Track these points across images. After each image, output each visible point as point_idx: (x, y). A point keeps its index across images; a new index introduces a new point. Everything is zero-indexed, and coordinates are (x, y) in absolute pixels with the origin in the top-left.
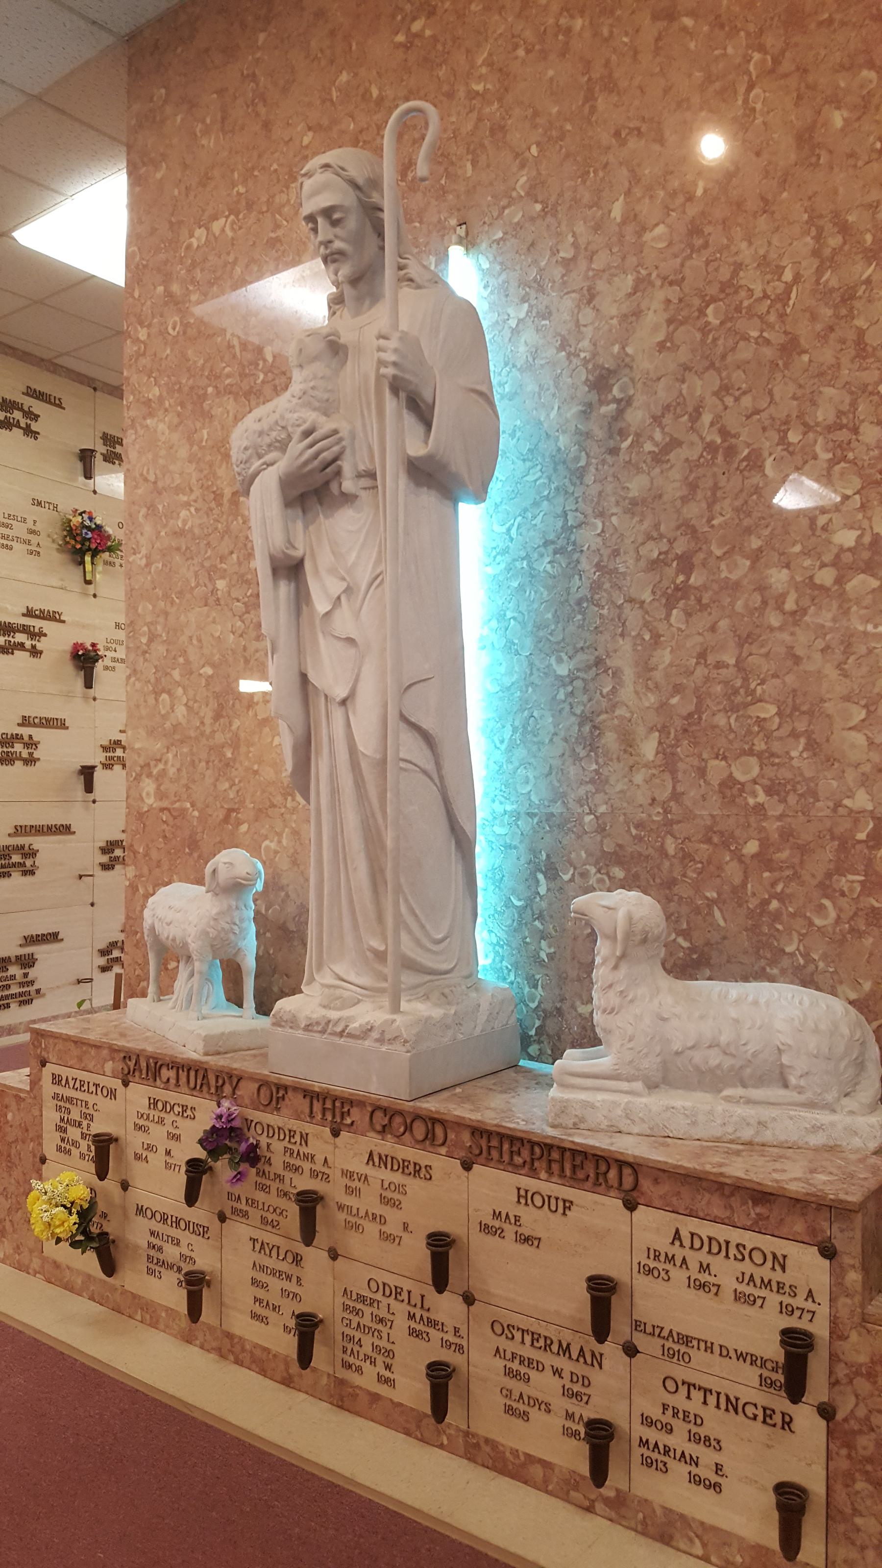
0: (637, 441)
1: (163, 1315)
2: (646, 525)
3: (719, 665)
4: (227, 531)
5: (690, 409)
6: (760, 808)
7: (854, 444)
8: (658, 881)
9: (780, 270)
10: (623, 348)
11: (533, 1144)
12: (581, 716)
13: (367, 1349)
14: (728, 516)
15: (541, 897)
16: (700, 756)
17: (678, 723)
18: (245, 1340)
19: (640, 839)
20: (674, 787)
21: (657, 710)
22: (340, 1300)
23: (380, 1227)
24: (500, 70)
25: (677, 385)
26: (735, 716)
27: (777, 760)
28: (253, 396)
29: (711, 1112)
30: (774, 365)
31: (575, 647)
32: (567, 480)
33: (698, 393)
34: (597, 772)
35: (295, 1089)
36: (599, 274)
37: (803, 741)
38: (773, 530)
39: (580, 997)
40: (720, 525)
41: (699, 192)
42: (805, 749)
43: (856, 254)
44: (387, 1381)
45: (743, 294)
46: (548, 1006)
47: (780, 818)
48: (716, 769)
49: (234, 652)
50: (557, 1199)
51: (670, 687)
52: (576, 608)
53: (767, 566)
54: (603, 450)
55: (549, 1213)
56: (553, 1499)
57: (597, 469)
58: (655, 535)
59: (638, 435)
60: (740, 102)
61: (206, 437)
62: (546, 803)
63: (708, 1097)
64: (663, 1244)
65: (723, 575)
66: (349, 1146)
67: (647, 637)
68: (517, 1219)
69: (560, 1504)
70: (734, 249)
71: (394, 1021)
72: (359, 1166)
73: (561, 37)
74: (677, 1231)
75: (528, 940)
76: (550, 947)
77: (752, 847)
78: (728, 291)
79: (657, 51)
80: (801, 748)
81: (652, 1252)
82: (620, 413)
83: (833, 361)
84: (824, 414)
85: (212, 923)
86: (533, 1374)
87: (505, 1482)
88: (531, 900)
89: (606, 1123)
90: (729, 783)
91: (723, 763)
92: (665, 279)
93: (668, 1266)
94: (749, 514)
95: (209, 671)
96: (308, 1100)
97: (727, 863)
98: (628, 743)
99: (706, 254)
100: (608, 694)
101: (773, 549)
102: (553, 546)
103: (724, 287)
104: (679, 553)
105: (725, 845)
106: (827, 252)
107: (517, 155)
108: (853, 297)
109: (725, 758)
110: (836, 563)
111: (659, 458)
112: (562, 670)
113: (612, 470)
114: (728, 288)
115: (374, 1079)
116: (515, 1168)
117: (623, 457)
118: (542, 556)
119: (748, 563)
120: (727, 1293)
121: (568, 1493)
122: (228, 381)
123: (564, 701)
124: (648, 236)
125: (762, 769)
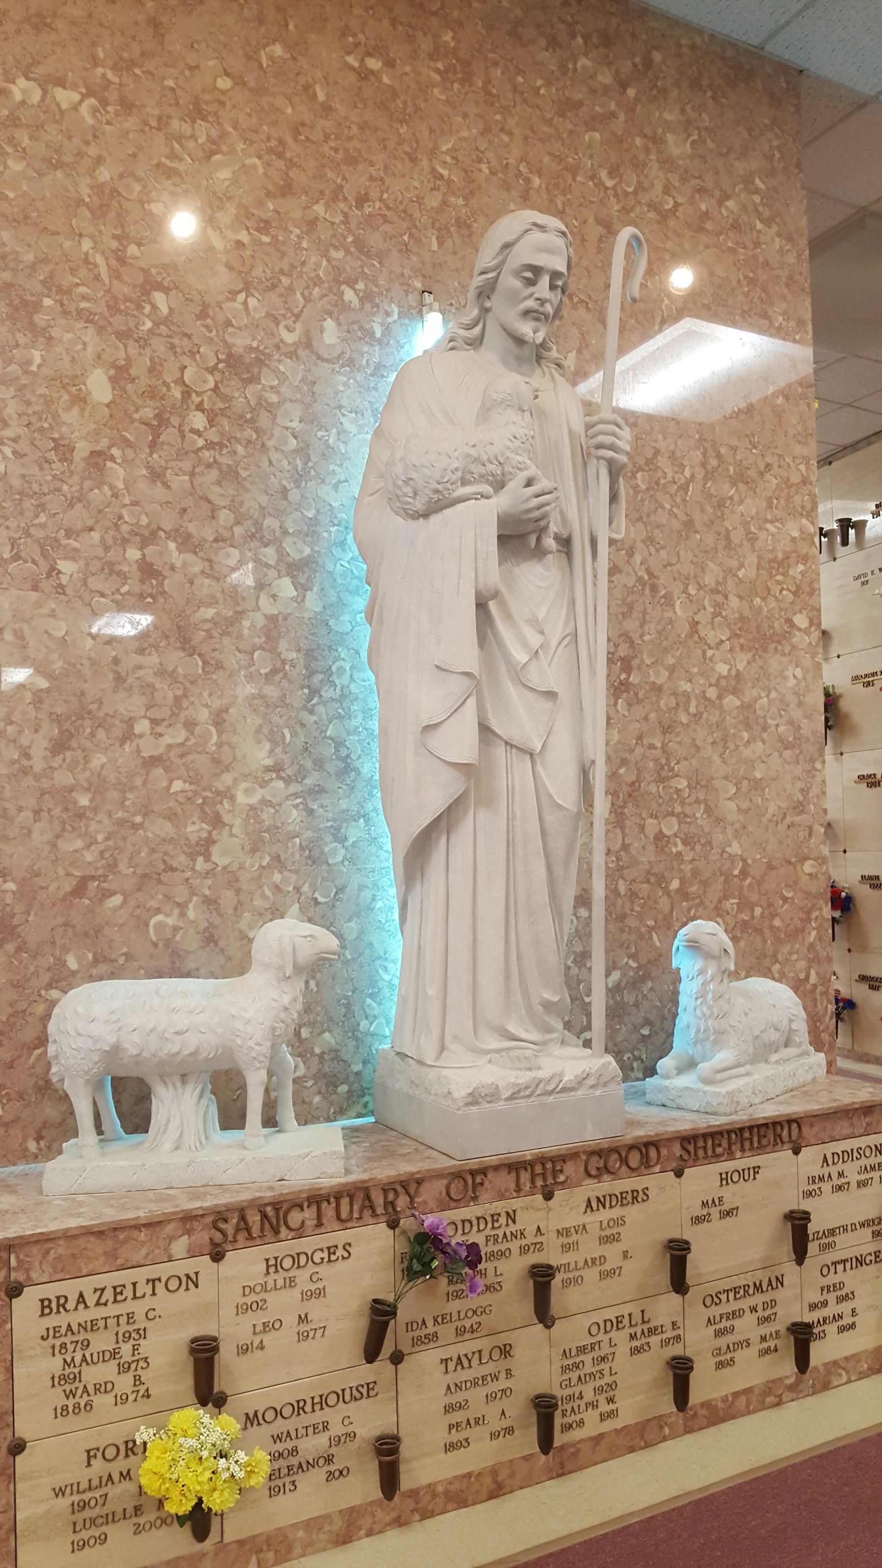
1: (301, 1534)
3: (652, 747)
4: (81, 498)
5: (627, 547)
6: (679, 854)
8: (614, 916)
11: (729, 1132)
13: (589, 1396)
17: (625, 789)
28: (131, 343)
35: (496, 1168)
37: (703, 806)
45: (660, 473)
49: (93, 663)
53: (678, 679)
61: (38, 360)
65: (652, 679)
66: (564, 1203)
68: (720, 1199)
69: (765, 1412)
77: (675, 884)
83: (713, 545)
84: (709, 580)
85: (283, 1015)
86: (736, 1323)
90: (660, 836)
96: (514, 1174)
103: (648, 462)
106: (709, 468)
109: (656, 817)
110: (717, 685)
115: (589, 1125)
120: (854, 1185)
122: (83, 305)
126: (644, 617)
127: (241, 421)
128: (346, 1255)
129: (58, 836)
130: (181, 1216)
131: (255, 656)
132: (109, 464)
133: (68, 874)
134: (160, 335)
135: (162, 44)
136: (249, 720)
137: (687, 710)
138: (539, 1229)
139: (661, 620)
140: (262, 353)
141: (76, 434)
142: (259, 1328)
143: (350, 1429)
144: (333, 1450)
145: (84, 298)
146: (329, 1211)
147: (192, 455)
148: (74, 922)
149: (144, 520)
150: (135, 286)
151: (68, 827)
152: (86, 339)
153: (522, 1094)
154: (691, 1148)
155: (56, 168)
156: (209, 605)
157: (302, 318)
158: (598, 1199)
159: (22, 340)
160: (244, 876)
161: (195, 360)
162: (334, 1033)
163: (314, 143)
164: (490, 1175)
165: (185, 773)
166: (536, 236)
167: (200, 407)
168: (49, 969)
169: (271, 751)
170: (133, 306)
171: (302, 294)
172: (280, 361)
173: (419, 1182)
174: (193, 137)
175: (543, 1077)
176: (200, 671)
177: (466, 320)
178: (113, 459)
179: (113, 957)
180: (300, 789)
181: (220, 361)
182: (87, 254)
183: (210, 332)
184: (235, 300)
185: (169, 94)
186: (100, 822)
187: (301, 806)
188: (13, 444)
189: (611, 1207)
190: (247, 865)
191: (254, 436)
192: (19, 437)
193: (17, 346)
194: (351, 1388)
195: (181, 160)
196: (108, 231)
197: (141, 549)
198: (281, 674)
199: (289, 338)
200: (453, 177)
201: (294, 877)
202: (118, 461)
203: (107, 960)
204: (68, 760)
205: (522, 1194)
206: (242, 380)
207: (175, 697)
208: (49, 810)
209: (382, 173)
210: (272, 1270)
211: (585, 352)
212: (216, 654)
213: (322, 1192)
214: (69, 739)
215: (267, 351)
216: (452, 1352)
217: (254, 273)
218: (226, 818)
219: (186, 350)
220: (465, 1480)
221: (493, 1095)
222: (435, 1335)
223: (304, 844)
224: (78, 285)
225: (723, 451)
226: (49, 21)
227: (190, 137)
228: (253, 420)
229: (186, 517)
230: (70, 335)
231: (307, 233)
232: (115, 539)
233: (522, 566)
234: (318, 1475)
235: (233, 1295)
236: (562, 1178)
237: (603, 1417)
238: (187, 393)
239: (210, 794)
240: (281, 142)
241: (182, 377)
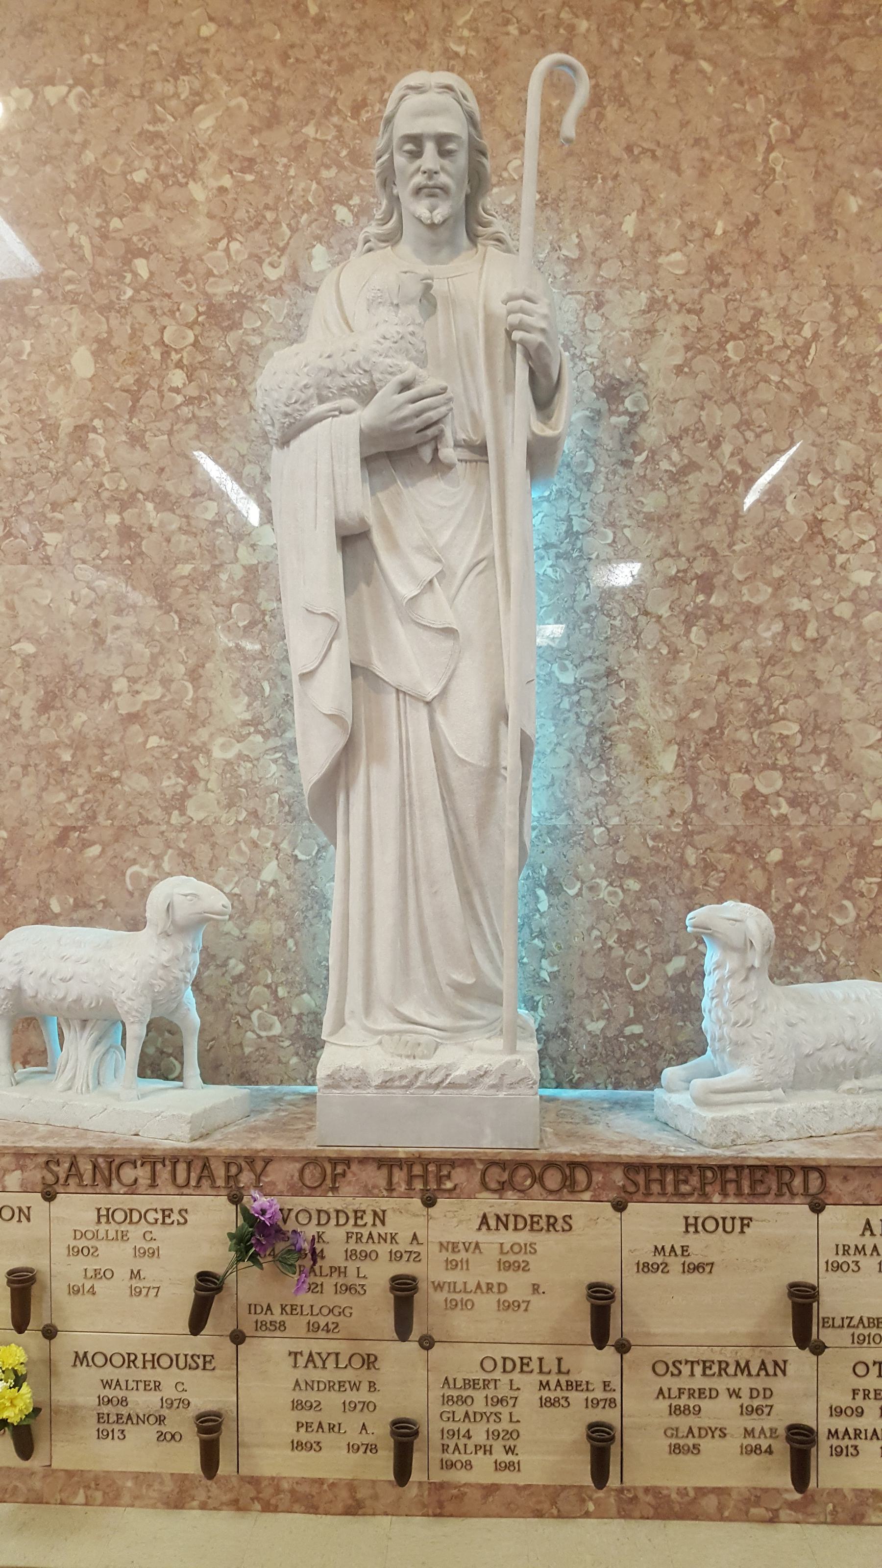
0: (653, 458)
1: (129, 1484)
2: (663, 541)
3: (742, 683)
4: (66, 472)
7: (869, 496)
9: (800, 325)
10: (637, 363)
11: (702, 1168)
12: (589, 726)
14: (750, 544)
15: (541, 915)
16: (722, 770)
17: (699, 737)
18: (281, 1479)
19: (656, 850)
20: (695, 799)
21: (676, 723)
22: (437, 1393)
23: (498, 1297)
24: (487, 40)
25: (696, 410)
26: (757, 732)
27: (799, 775)
28: (113, 314)
29: (843, 1107)
30: (794, 412)
31: (582, 656)
32: (571, 485)
33: (718, 423)
34: (608, 784)
35: (363, 1161)
36: (608, 282)
37: (824, 757)
38: (794, 563)
39: (590, 1014)
40: (741, 551)
41: (719, 231)
42: (826, 765)
43: (870, 328)
44: (509, 1466)
45: (763, 338)
46: (550, 1028)
47: (803, 827)
48: (739, 782)
50: (733, 1219)
51: (690, 702)
52: (583, 616)
53: (788, 595)
54: (613, 460)
55: (724, 1234)
56: (733, 1524)
57: (607, 478)
58: (673, 552)
59: (653, 453)
60: (760, 159)
61: (28, 349)
62: (547, 815)
63: (829, 1093)
64: (853, 1238)
65: (745, 599)
66: (451, 1214)
67: (665, 651)
68: (684, 1249)
69: (746, 1526)
70: (754, 295)
71: (517, 1062)
72: (468, 1233)
73: (562, 31)
74: (868, 1222)
75: (525, 960)
76: (552, 965)
77: (776, 855)
78: (748, 332)
79: (673, 83)
80: (823, 763)
81: (841, 1248)
82: (631, 429)
83: (849, 419)
84: (841, 464)
85: (160, 972)
86: (705, 1404)
87: (675, 1526)
88: (529, 918)
89: (760, 1134)
90: (751, 795)
91: (746, 776)
92: (682, 305)
93: (857, 1258)
94: (771, 545)
95: (30, 648)
96: (384, 1171)
97: (751, 871)
98: (643, 752)
99: (725, 293)
100: (620, 705)
101: (794, 579)
102: (555, 550)
103: (743, 328)
104: (699, 573)
105: (749, 853)
106: (844, 320)
107: (508, 136)
108: (867, 365)
109: (747, 771)
111: (678, 476)
112: (568, 678)
113: (625, 481)
114: (749, 329)
115: (488, 1131)
116: (682, 1197)
117: (637, 470)
118: (542, 558)
119: (770, 590)
121: (747, 1513)
122: (69, 287)
123: (569, 711)
124: (663, 260)
125: (785, 782)
126: (735, 522)
127: (222, 370)
128: (182, 1221)
129: (44, 789)
130: (12, 1151)
131: (233, 610)
132: (92, 436)
133: (52, 825)
134: (140, 301)
135: (146, 11)
136: (226, 674)
137: (801, 634)
138: (415, 1237)
139: (763, 522)
140: (245, 297)
141: (62, 412)
142: (90, 1273)
143: (184, 1396)
144: (165, 1412)
145: (70, 281)
146: (164, 1174)
147: (171, 414)
148: (58, 869)
149: (123, 485)
150: (116, 259)
151: (52, 781)
152: (72, 320)
153: (397, 1083)
154: (641, 1179)
155: (45, 164)
156: (186, 561)
157: (288, 251)
158: (498, 1218)
159: (14, 333)
160: (220, 831)
161: (174, 318)
162: (315, 995)
163: (305, 62)
164: (354, 1167)
165: (161, 729)
166: (414, 101)
167: (179, 365)
168: (35, 910)
169: (249, 705)
170: (115, 278)
171: (289, 225)
172: (263, 301)
173: (268, 1161)
174: (176, 95)
175: (425, 1067)
176: (177, 628)
177: (378, 214)
178: (94, 430)
179: (92, 903)
180: (280, 743)
181: (199, 314)
182: (72, 239)
183: (190, 286)
184: (216, 249)
185: (152, 58)
186: (80, 776)
187: (281, 761)
188: (7, 432)
189: (516, 1229)
190: (223, 820)
191: (235, 383)
192: (11, 423)
193: (10, 339)
194: (186, 1355)
195: (162, 121)
196: (92, 210)
197: (120, 513)
198: (260, 626)
199: (273, 274)
200: (471, 51)
201: (272, 834)
202: (100, 431)
203: (87, 906)
204: (53, 718)
205: (395, 1194)
206: (222, 329)
207: (152, 654)
208: (36, 765)
209: (383, 72)
210: (103, 1220)
211: (649, 210)
212: (193, 609)
213: (154, 1153)
214: (53, 700)
215: (249, 294)
216: (305, 1346)
217: (236, 216)
218: (202, 773)
219: (166, 310)
220: (317, 1485)
221: (361, 1080)
222: (283, 1324)
223: (283, 799)
224: (64, 269)
225: (866, 295)
226: (40, 26)
227: (173, 96)
228: (234, 367)
229: (164, 476)
230: (56, 320)
231: (295, 159)
232: (96, 506)
233: (419, 484)
234: (150, 1431)
235: (63, 1239)
236: (449, 1185)
237: (499, 1467)
238: (167, 351)
239: (184, 749)
240: (268, 72)
241: (162, 338)
